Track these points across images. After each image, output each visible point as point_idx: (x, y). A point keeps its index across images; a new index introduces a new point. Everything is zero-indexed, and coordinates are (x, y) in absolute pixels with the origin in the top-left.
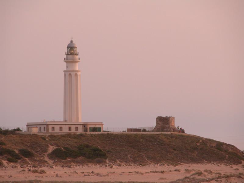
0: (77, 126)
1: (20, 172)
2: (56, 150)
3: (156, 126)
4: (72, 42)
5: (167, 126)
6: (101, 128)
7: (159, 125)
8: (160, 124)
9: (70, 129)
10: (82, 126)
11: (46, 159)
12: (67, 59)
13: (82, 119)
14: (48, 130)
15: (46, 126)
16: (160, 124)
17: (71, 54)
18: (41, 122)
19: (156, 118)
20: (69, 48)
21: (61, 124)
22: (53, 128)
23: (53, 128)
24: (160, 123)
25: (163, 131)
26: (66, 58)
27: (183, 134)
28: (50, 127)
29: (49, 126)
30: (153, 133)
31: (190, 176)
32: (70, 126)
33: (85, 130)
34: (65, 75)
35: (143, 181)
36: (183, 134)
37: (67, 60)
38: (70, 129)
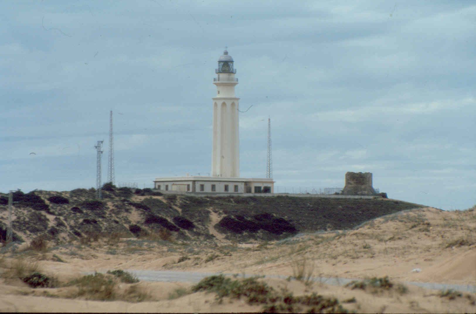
0: (166, 184)
1: (41, 280)
2: (225, 218)
3: (345, 187)
4: (226, 53)
5: (363, 187)
6: (270, 187)
7: (350, 186)
8: (351, 184)
9: (226, 188)
10: (243, 183)
11: (212, 231)
12: (219, 80)
13: (244, 175)
14: (194, 188)
15: (191, 184)
16: (351, 184)
17: (224, 72)
18: (207, 176)
19: (346, 175)
20: (222, 63)
21: (187, 179)
22: (202, 186)
23: (202, 186)
24: (352, 182)
25: (356, 194)
26: (217, 79)
27: (385, 199)
28: (198, 185)
29: (196, 182)
30: (340, 197)
31: (344, 302)
32: (226, 183)
33: (249, 190)
34: (216, 104)
35: (239, 312)
36: (385, 199)
37: (220, 82)
38: (226, 188)
